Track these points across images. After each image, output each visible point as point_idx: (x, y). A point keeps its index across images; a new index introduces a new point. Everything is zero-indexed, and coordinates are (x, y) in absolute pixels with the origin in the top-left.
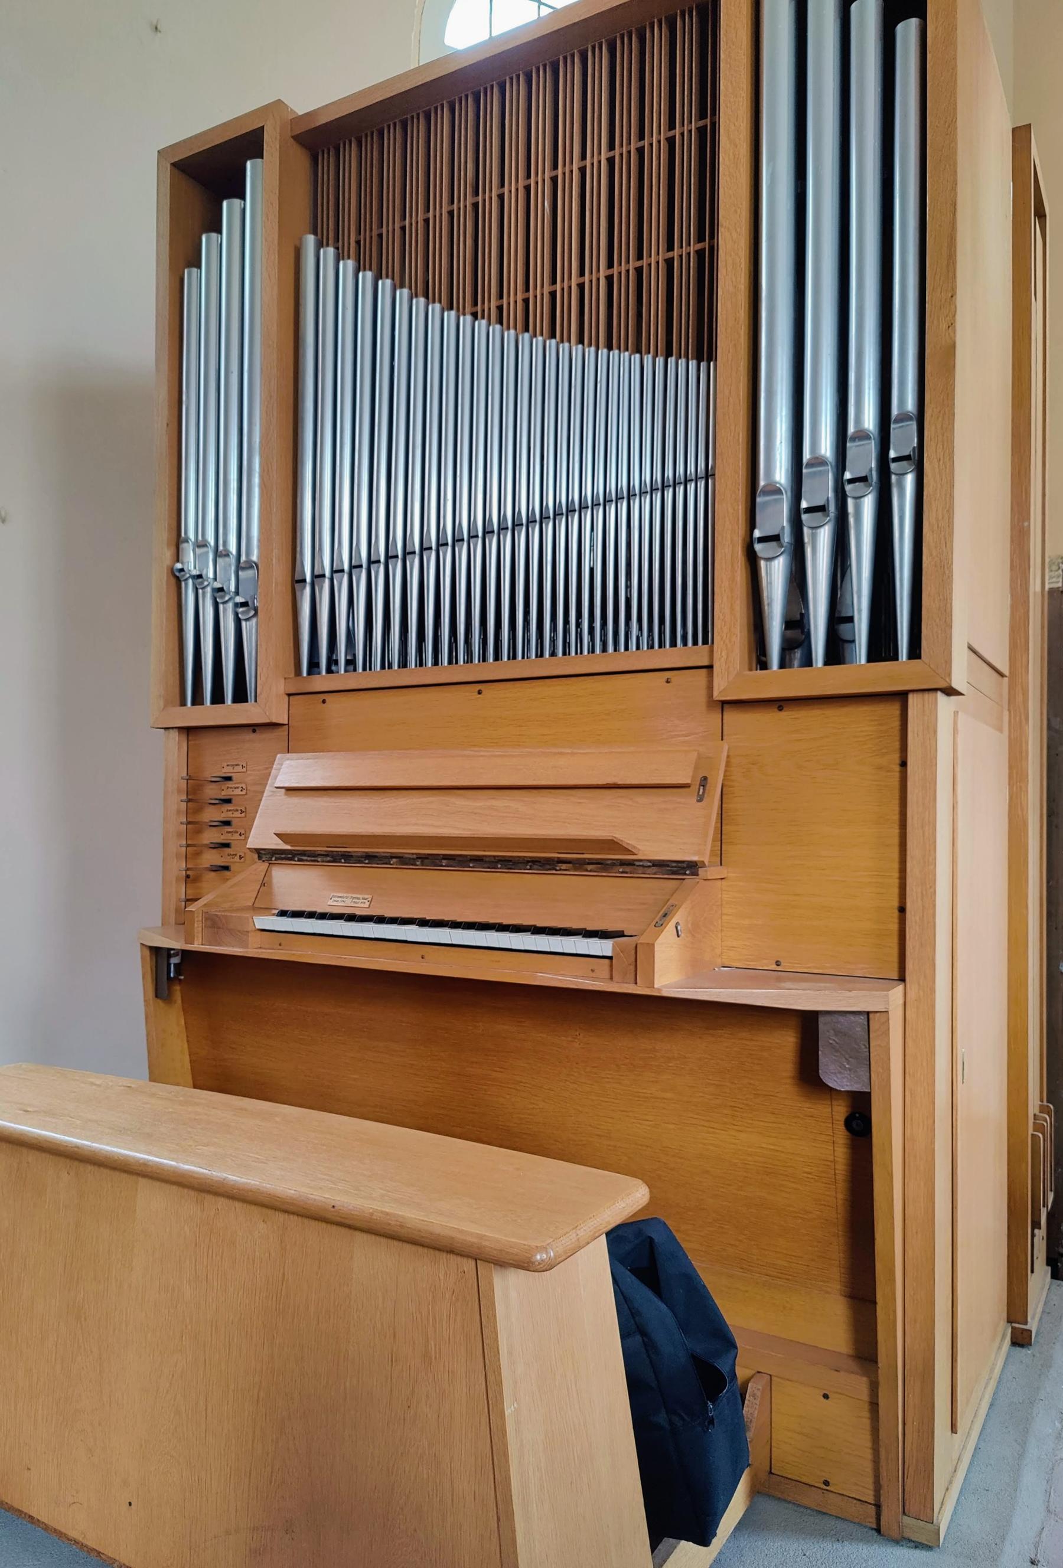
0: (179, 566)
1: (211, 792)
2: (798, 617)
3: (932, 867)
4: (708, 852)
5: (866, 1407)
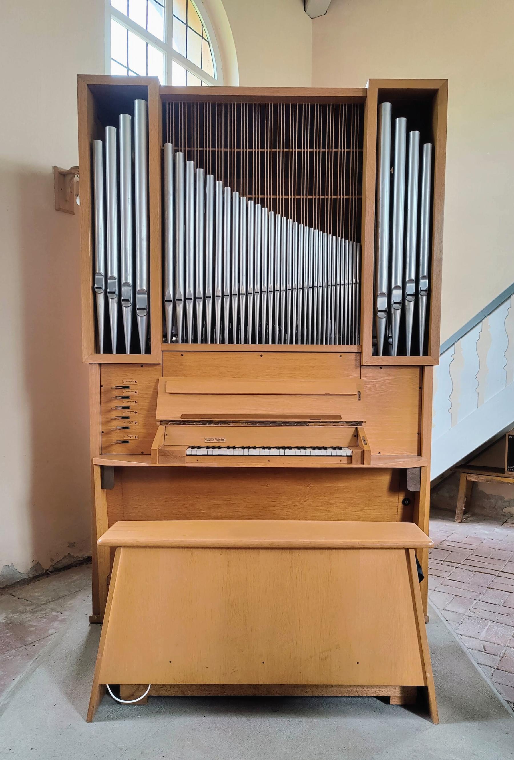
3: (431, 421)
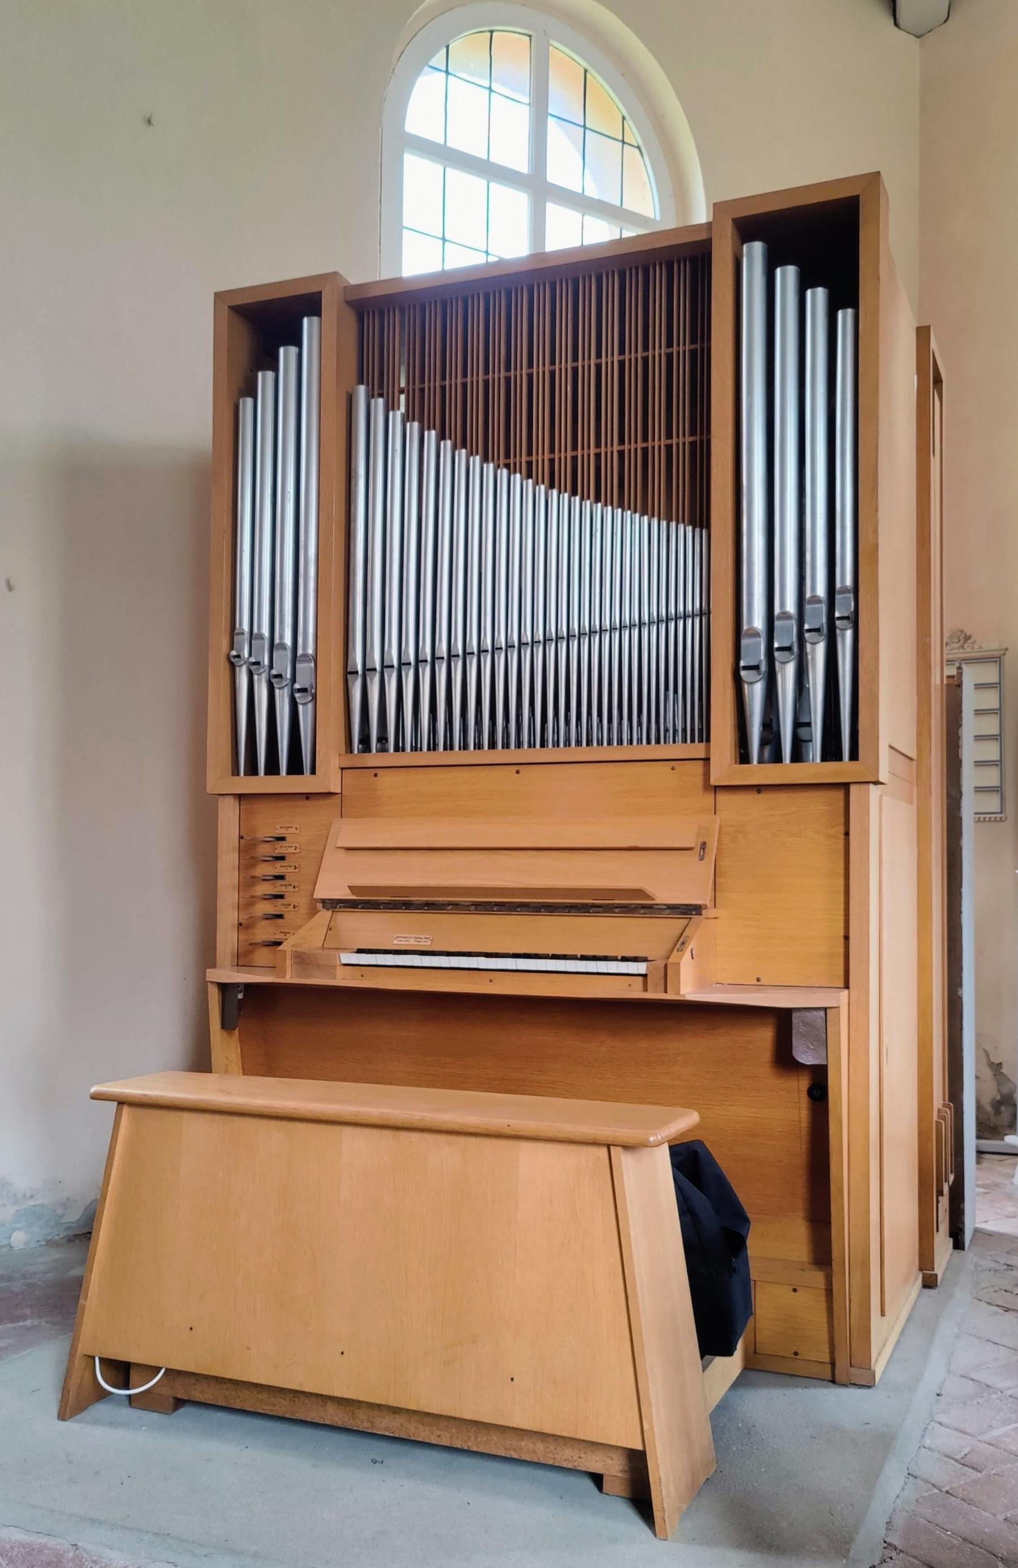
0: (234, 653)
1: (264, 850)
2: (769, 722)
4: (709, 900)
5: (823, 1293)
